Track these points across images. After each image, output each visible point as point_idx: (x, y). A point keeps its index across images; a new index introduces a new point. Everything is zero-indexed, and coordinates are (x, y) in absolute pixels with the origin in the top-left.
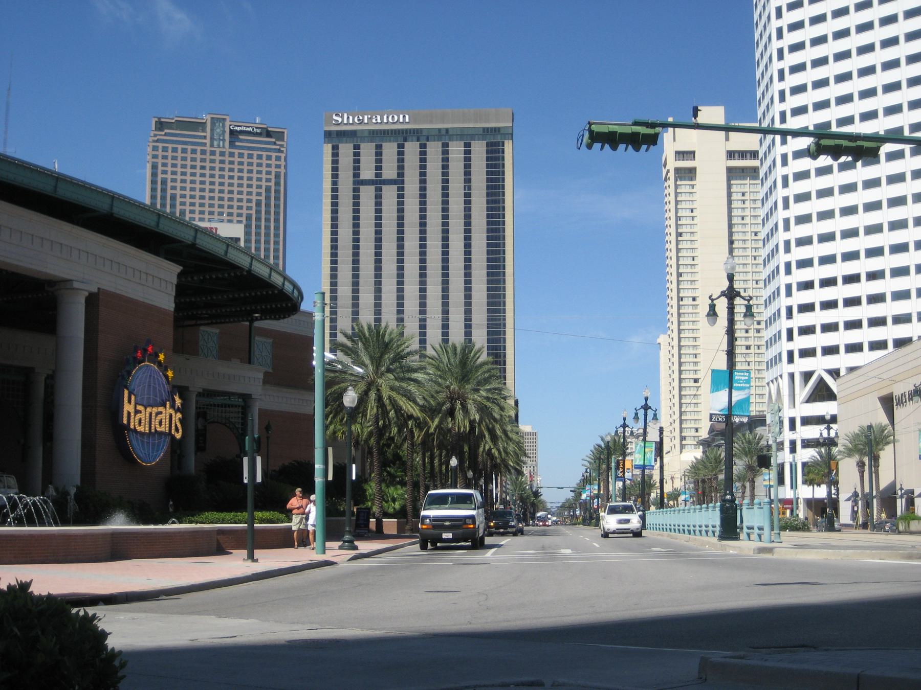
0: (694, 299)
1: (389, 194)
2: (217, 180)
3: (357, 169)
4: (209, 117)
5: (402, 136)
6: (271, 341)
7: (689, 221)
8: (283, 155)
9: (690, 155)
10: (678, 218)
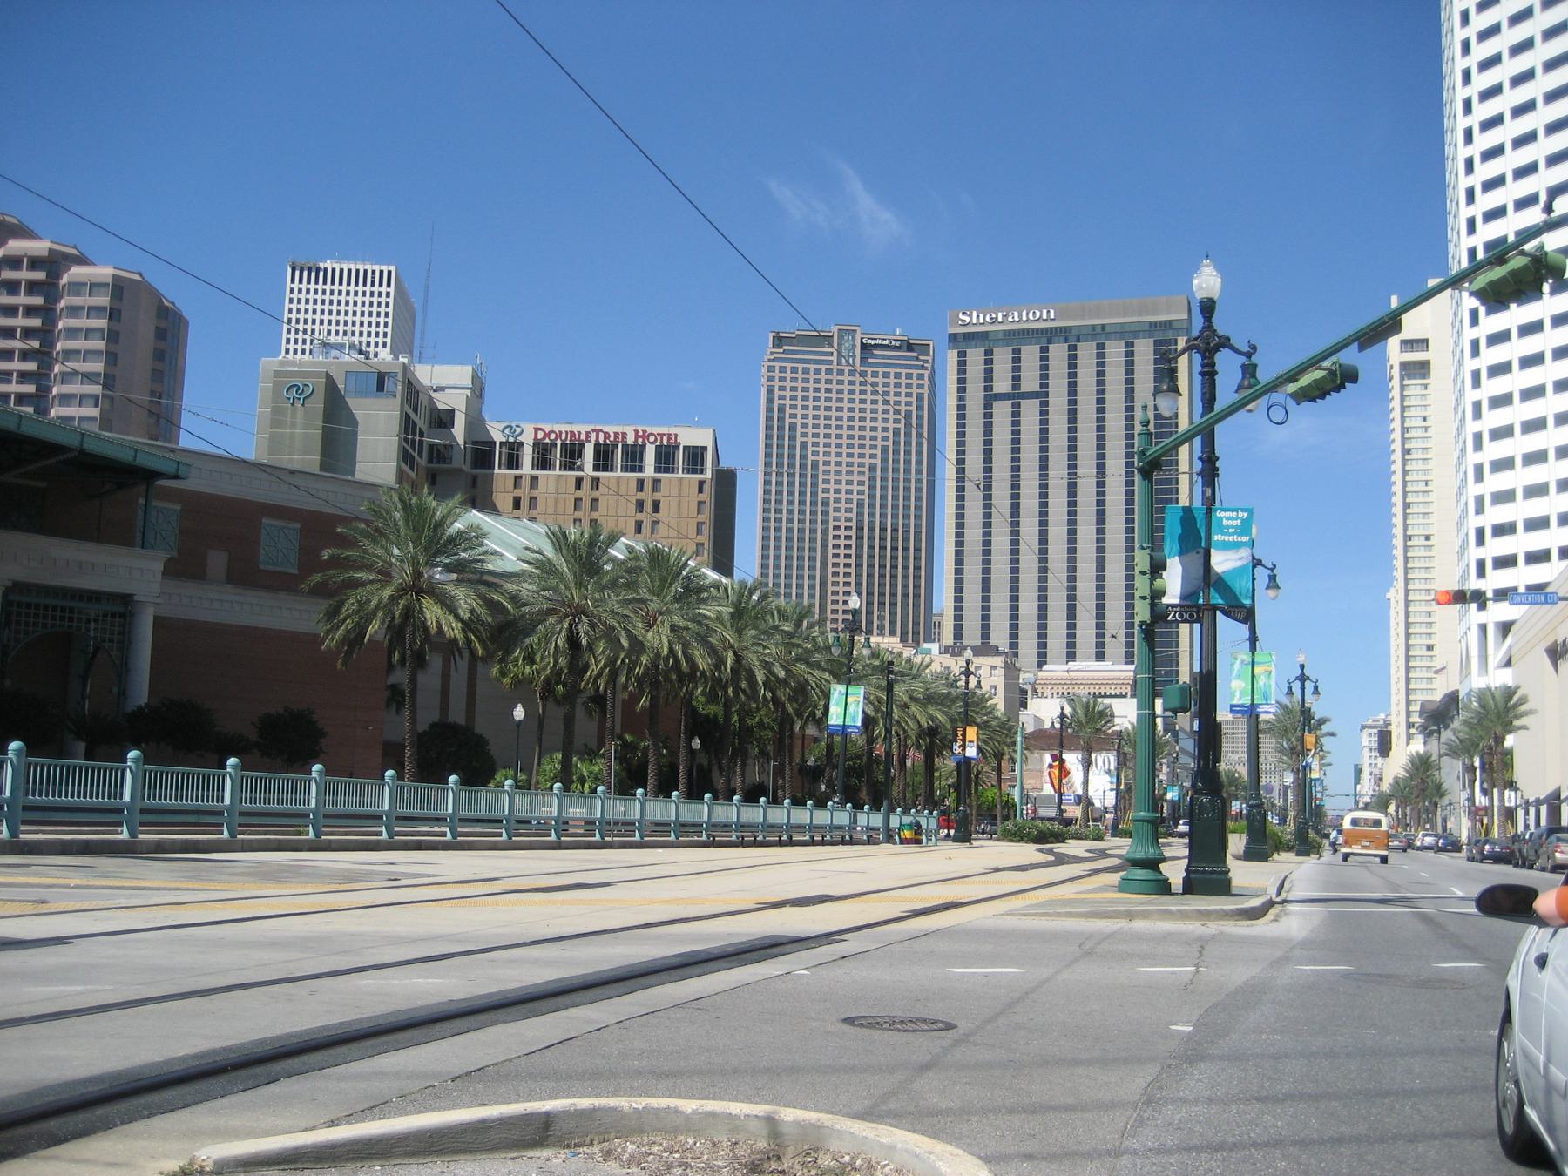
0: (1428, 538)
1: (1030, 409)
2: (846, 405)
3: (988, 380)
4: (834, 329)
5: (1045, 337)
6: (298, 526)
7: (1420, 433)
8: (926, 373)
9: (1423, 343)
10: (1404, 430)
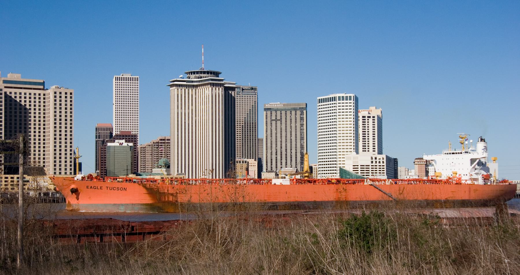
1: (279, 122)
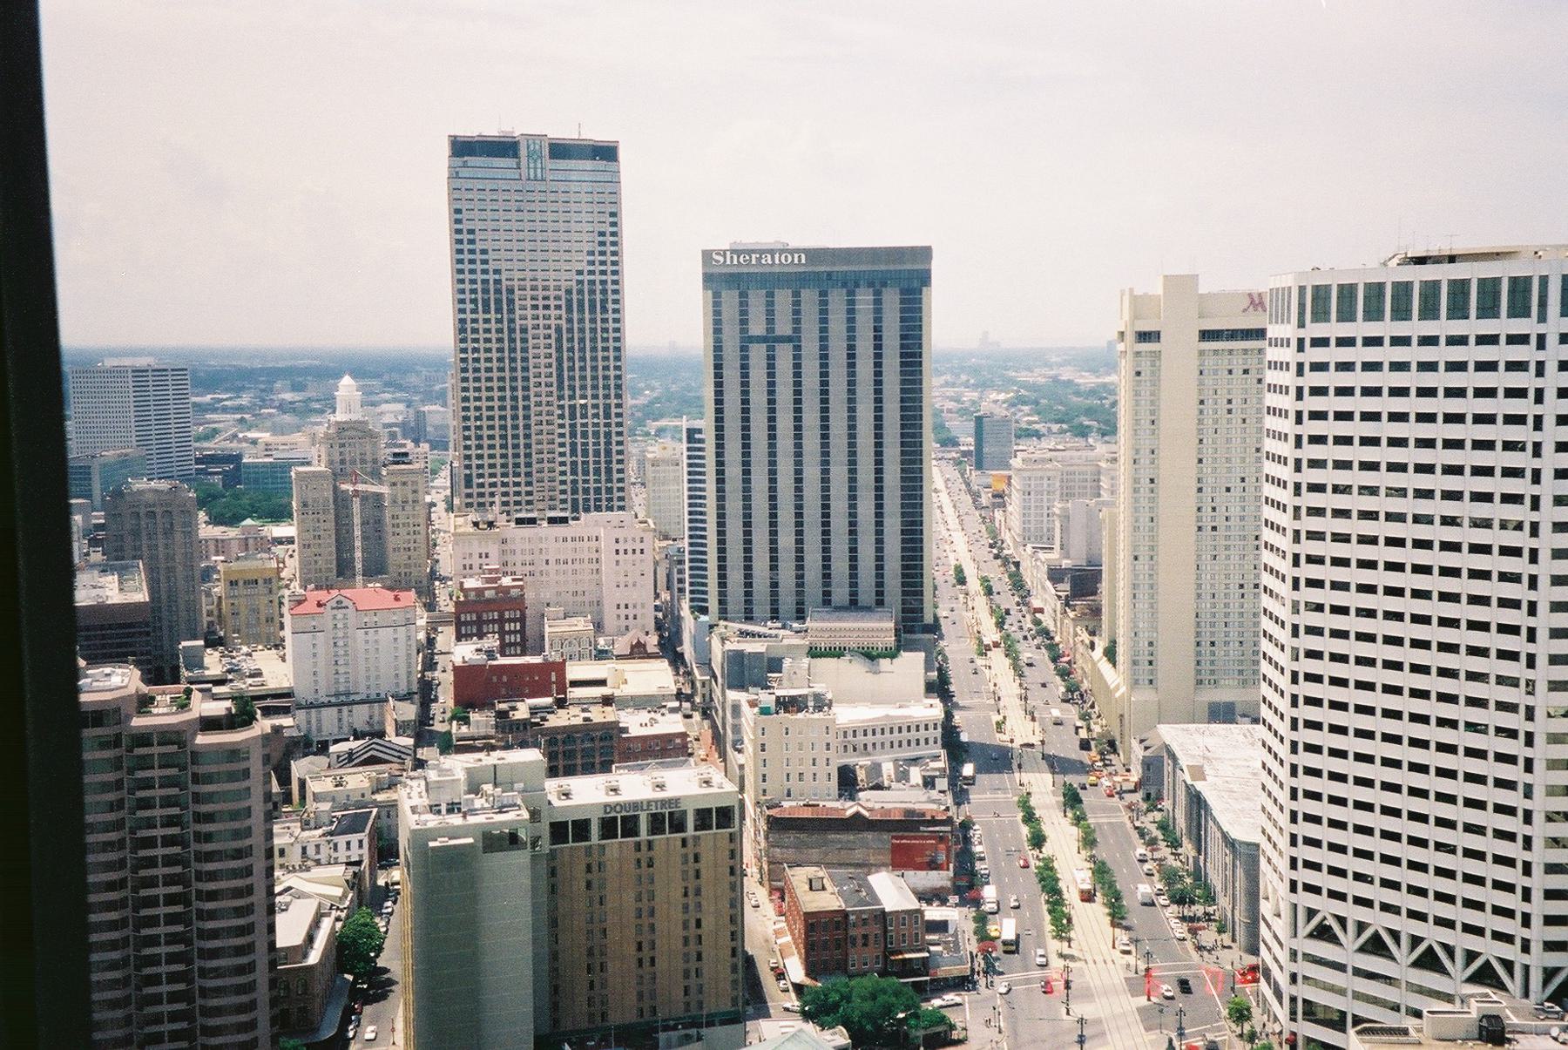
3: (744, 322)
